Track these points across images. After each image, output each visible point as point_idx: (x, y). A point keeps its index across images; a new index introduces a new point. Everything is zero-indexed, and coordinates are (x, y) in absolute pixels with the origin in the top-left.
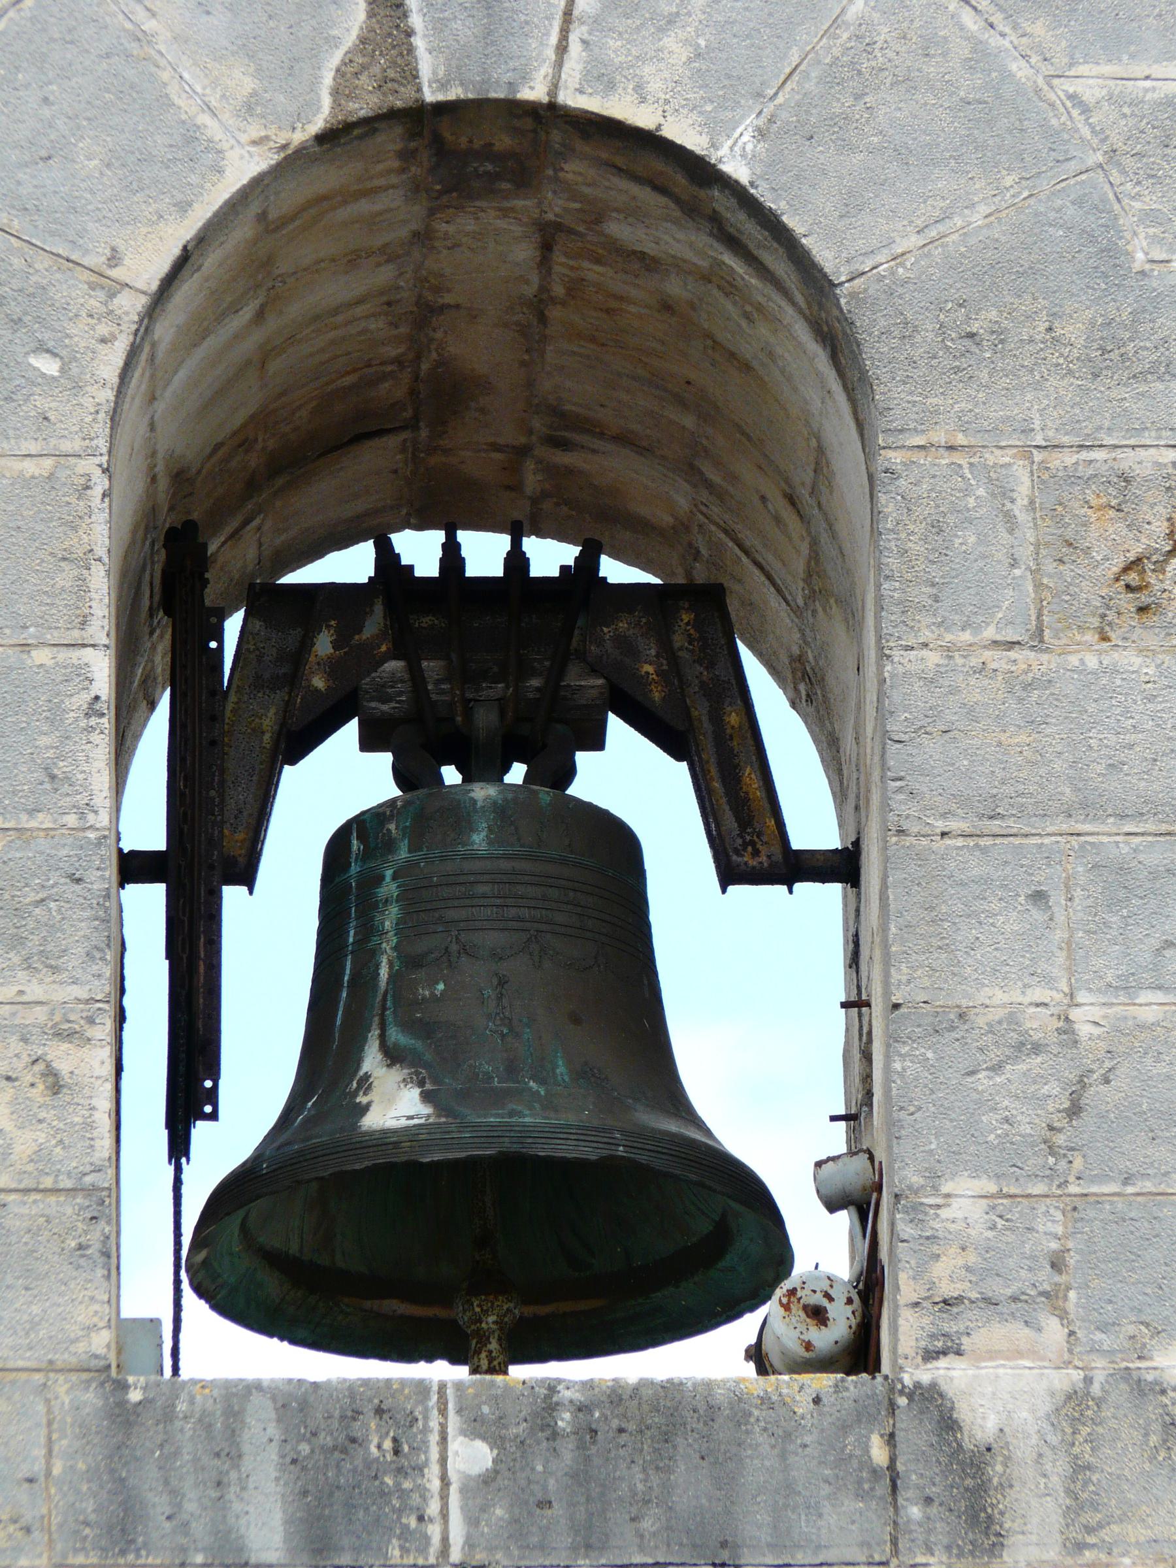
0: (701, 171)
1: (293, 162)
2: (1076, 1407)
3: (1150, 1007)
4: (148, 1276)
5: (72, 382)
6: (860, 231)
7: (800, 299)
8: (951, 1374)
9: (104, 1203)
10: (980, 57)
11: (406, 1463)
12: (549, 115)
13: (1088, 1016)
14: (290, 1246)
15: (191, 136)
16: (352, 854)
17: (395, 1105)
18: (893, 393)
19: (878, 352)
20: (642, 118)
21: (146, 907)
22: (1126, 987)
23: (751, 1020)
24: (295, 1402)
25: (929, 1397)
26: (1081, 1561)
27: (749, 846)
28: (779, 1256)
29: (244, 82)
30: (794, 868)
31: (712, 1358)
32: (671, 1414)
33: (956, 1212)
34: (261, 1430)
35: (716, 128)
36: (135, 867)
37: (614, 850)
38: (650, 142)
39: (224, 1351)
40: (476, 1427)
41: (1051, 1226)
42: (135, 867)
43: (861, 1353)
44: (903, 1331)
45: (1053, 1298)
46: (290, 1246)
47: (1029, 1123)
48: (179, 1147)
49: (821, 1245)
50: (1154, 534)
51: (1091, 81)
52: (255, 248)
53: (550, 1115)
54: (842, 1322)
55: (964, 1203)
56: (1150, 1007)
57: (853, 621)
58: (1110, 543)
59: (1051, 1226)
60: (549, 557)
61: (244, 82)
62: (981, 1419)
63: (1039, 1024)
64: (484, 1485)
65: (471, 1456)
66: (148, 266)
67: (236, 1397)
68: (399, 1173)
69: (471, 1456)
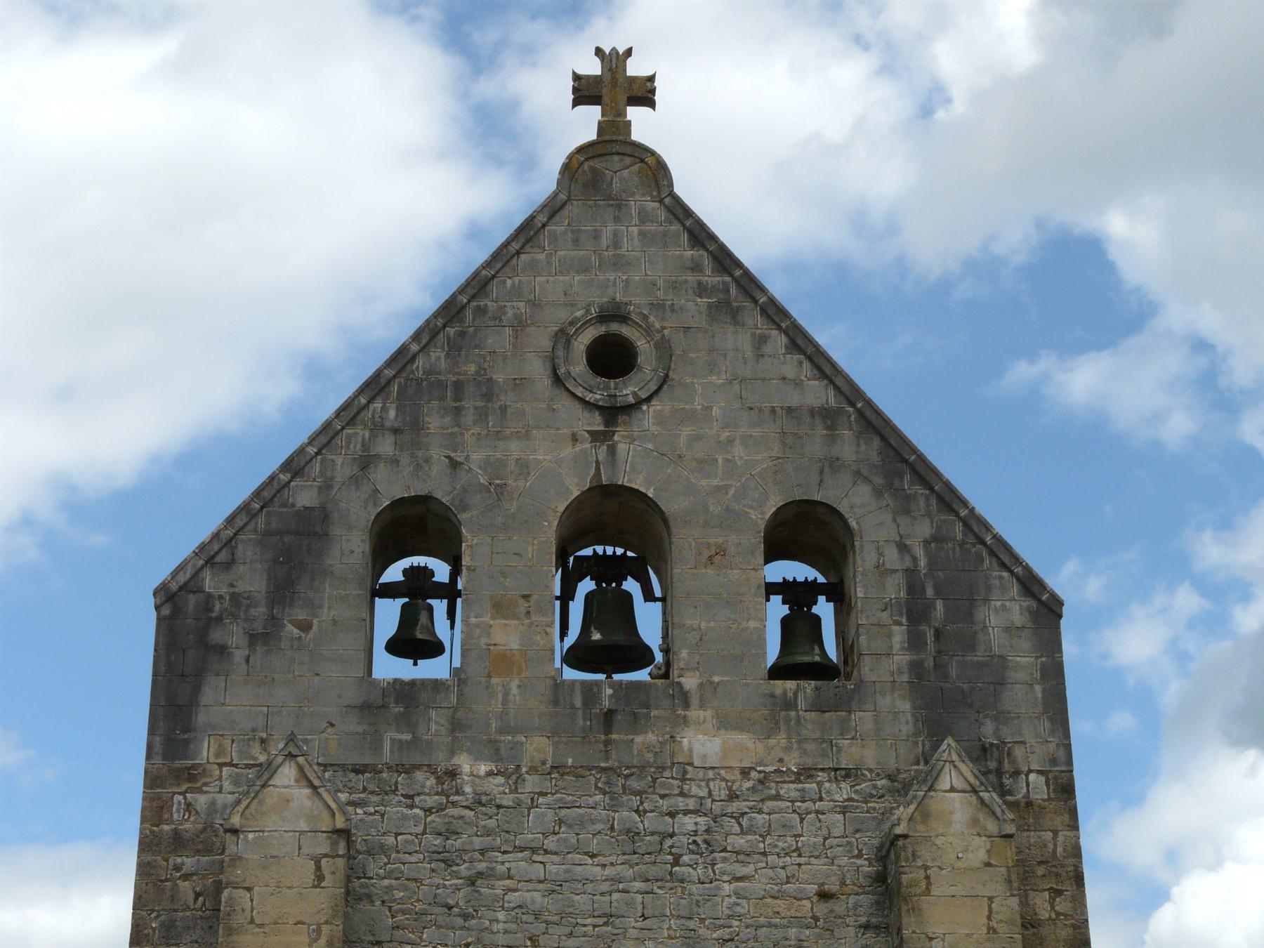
0: (645, 496)
1: (583, 493)
2: (701, 686)
3: (712, 624)
4: (558, 664)
5: (550, 526)
6: (670, 506)
7: (484, 272)
8: (682, 680)
9: (553, 652)
10: (687, 479)
11: (600, 692)
12: (622, 486)
13: (703, 626)
14: (579, 657)
15: (568, 488)
16: (589, 597)
17: (596, 636)
18: (674, 530)
19: (672, 523)
20: (636, 487)
21: (558, 603)
22: (709, 621)
23: (649, 621)
24: (583, 683)
25: (679, 684)
26: (406, 563)
27: (649, 596)
28: (653, 659)
29: (576, 481)
30: (655, 600)
31: (642, 675)
32: (638, 685)
33: (683, 655)
34: (578, 687)
35: (648, 489)
36: (557, 598)
37: (628, 597)
38: (637, 491)
39: (570, 674)
40: (610, 687)
41: (697, 657)
42: (557, 598)
43: (666, 676)
44: (675, 673)
45: (697, 669)
46: (579, 657)
47: (694, 642)
48: (562, 640)
49: (659, 657)
50: (713, 552)
51: (704, 482)
52: (576, 506)
53: (619, 638)
54: (663, 669)
55: (684, 654)
56: (712, 624)
57: (666, 562)
58: (706, 554)
59: (697, 657)
60: (619, 551)
61: (576, 481)
62: (687, 687)
63: (695, 626)
64: (610, 696)
65: (609, 691)
66: (561, 508)
67: (574, 682)
68: (597, 646)
69: (609, 691)
